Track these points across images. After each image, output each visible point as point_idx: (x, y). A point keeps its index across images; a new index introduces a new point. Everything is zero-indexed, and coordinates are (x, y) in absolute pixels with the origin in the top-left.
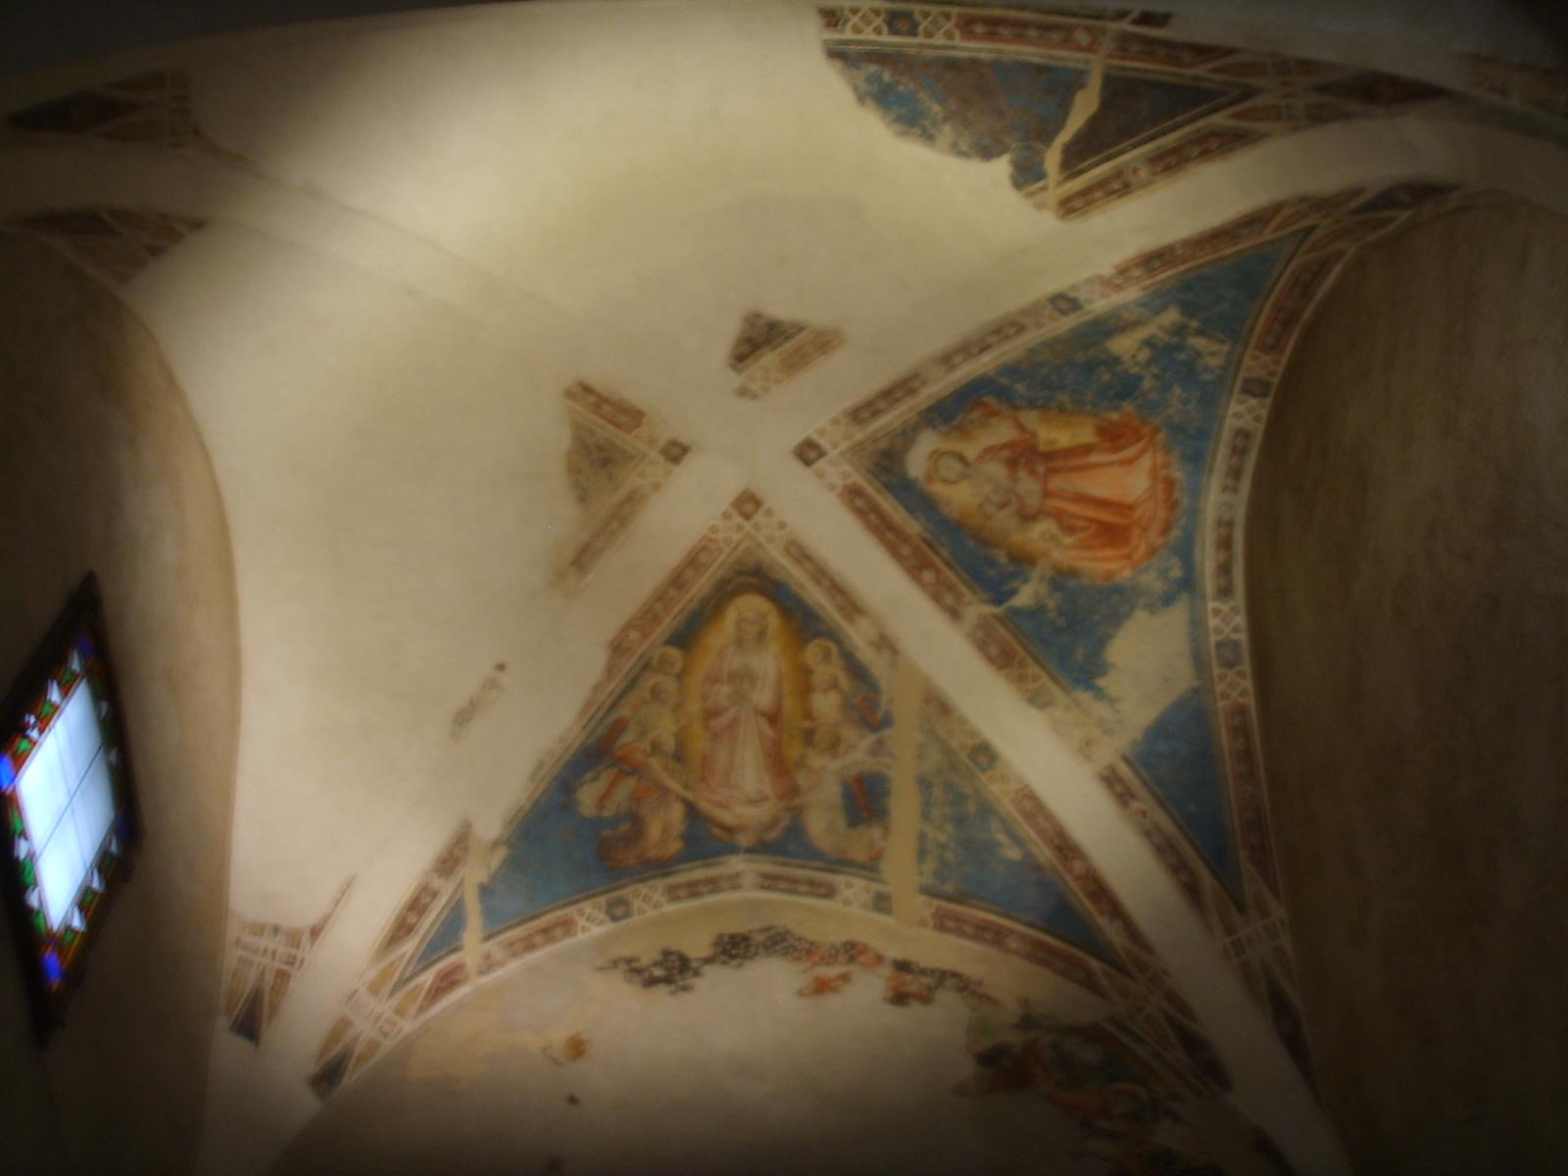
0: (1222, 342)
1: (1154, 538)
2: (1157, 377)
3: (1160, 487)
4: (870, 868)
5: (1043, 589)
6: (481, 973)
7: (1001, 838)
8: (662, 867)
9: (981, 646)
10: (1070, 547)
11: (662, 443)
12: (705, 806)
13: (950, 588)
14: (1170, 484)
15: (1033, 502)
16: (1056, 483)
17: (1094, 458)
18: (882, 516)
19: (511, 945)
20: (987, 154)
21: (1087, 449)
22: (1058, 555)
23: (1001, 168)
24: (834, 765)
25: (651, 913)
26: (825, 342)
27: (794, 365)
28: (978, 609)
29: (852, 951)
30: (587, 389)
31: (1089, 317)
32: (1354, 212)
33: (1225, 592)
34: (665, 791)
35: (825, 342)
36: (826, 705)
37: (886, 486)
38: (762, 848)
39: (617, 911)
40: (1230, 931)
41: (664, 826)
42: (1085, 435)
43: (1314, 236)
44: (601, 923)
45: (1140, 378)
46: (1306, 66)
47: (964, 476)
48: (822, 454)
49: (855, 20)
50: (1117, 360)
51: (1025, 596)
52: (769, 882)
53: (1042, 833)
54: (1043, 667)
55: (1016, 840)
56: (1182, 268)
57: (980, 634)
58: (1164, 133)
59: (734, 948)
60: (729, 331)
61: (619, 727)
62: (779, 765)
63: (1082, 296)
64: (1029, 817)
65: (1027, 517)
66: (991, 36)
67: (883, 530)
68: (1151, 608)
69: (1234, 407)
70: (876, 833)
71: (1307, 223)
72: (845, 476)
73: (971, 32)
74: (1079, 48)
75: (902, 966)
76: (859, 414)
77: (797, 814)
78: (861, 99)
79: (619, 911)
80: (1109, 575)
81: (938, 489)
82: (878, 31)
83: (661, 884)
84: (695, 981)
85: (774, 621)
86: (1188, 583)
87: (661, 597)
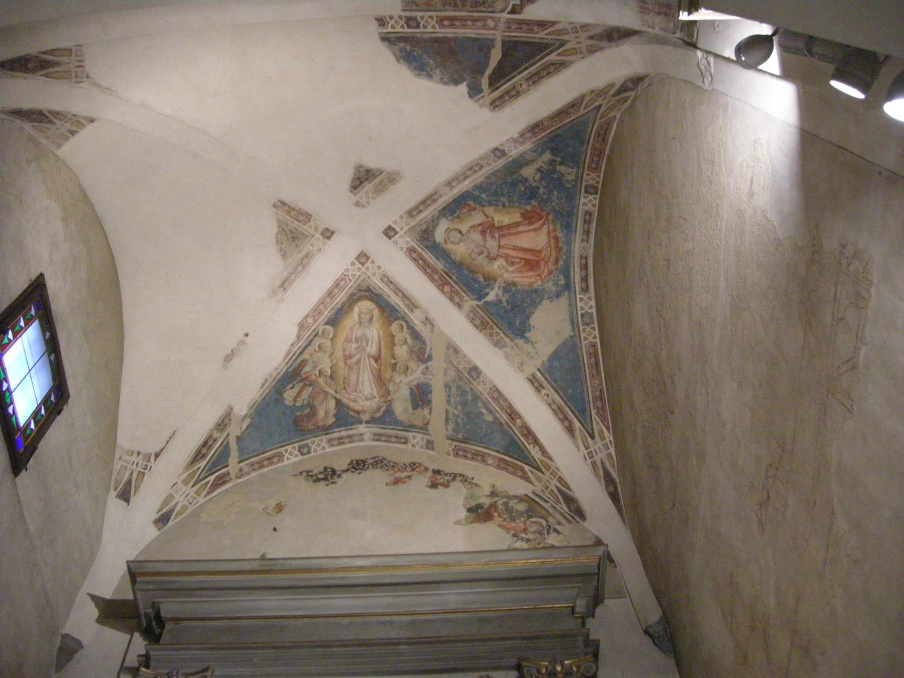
0: (572, 168)
1: (551, 266)
2: (545, 187)
3: (552, 242)
4: (424, 428)
5: (500, 293)
6: (237, 478)
7: (484, 411)
8: (326, 430)
9: (472, 321)
10: (513, 272)
11: (321, 230)
12: (344, 400)
13: (458, 294)
14: (556, 239)
15: (494, 251)
16: (504, 241)
17: (521, 229)
18: (424, 261)
19: (252, 465)
20: (456, 82)
21: (517, 224)
22: (506, 276)
23: (463, 88)
24: (406, 380)
25: (320, 452)
26: (393, 178)
27: (380, 189)
28: (470, 303)
29: (413, 466)
30: (284, 204)
31: (511, 159)
32: (614, 96)
33: (585, 290)
34: (327, 393)
35: (393, 178)
36: (401, 352)
37: (427, 247)
38: (372, 421)
39: (304, 450)
40: (587, 447)
41: (326, 411)
42: (517, 218)
43: (602, 110)
44: (296, 456)
45: (538, 188)
46: (585, 27)
47: (461, 240)
48: (396, 233)
49: (392, 22)
50: (526, 180)
51: (491, 297)
52: (377, 437)
53: (502, 408)
54: (500, 329)
55: (490, 412)
56: (548, 131)
57: (471, 315)
58: (531, 66)
59: (358, 466)
60: (348, 175)
61: (304, 363)
62: (380, 380)
63: (506, 148)
64: (496, 400)
65: (492, 259)
66: (452, 26)
67: (425, 267)
68: (550, 299)
69: (582, 200)
70: (426, 411)
71: (597, 104)
72: (407, 243)
73: (443, 25)
74: (490, 29)
75: (437, 472)
76: (410, 213)
77: (390, 403)
78: (398, 60)
79: (305, 451)
80: (531, 285)
81: (449, 246)
82: (402, 27)
83: (325, 438)
84: (338, 480)
85: (376, 312)
86: (568, 286)
87: (322, 302)
